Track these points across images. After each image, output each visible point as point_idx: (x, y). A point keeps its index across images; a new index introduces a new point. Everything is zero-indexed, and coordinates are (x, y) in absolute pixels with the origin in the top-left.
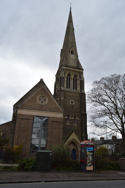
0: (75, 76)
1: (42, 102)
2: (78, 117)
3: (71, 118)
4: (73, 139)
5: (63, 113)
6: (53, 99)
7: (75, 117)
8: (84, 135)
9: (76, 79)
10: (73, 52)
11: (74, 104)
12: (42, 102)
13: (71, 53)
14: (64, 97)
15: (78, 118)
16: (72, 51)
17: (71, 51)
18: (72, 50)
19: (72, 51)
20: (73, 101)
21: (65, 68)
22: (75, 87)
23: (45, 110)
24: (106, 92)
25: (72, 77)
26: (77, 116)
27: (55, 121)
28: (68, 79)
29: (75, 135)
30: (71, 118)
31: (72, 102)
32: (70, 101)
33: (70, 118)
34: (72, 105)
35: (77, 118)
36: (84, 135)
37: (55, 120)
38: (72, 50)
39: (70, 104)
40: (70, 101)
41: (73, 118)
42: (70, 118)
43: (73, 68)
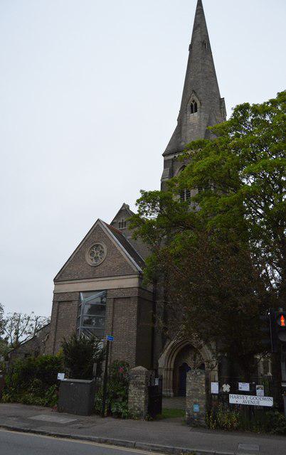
1: (96, 258)
5: (137, 276)
13: (189, 112)
17: (192, 106)
18: (193, 101)
37: (119, 296)
38: (193, 101)
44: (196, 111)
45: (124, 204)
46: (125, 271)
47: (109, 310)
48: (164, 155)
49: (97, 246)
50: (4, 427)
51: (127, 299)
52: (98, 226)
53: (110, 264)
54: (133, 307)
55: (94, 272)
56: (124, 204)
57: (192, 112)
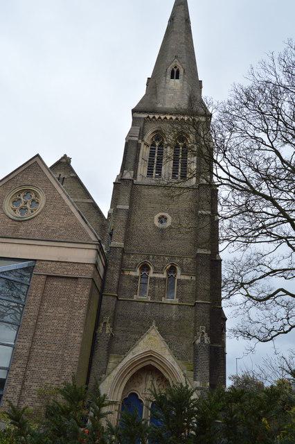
0: (182, 137)
1: (23, 209)
2: (182, 270)
3: (157, 275)
4: (150, 356)
5: (94, 247)
6: (64, 197)
7: (172, 269)
8: (203, 341)
9: (185, 146)
10: (178, 72)
11: (168, 224)
12: (23, 209)
13: (169, 76)
14: (131, 204)
15: (183, 273)
16: (175, 70)
17: (173, 72)
18: (176, 67)
19: (175, 70)
20: (166, 215)
21: (145, 116)
22: (180, 169)
23: (28, 238)
24: (273, 147)
25: (170, 138)
26: (181, 266)
27: (59, 276)
28: (156, 151)
29: (159, 338)
30: (157, 275)
31: (162, 219)
32: (156, 217)
33: (151, 275)
34: (162, 230)
35: (179, 276)
36: (203, 341)
37: (58, 273)
38: (176, 67)
39: (154, 226)
40: (156, 217)
41: (164, 276)
42: (151, 275)
43: (171, 114)
44: (177, 78)
45: (65, 155)
46: (75, 239)
47: (35, 293)
48: (64, 164)
49: (28, 191)
50: (2, 237)
51: (69, 282)
52: (36, 162)
53: (49, 221)
54: (82, 294)
55: (16, 230)
56: (65, 155)
57: (172, 78)
